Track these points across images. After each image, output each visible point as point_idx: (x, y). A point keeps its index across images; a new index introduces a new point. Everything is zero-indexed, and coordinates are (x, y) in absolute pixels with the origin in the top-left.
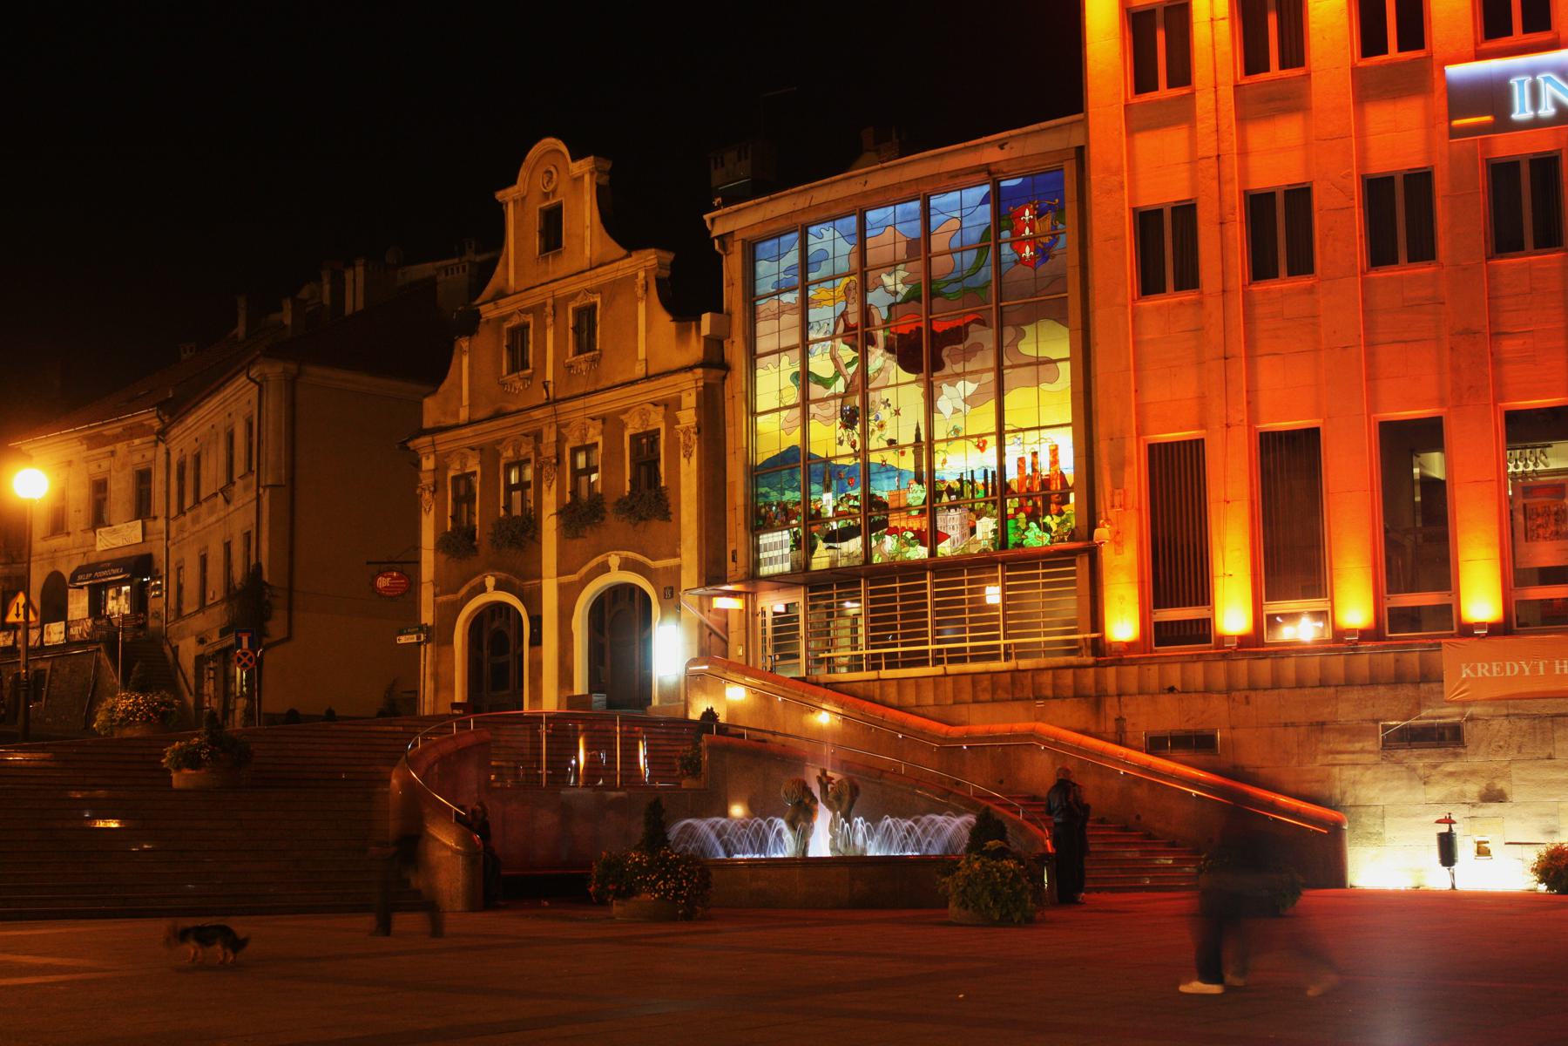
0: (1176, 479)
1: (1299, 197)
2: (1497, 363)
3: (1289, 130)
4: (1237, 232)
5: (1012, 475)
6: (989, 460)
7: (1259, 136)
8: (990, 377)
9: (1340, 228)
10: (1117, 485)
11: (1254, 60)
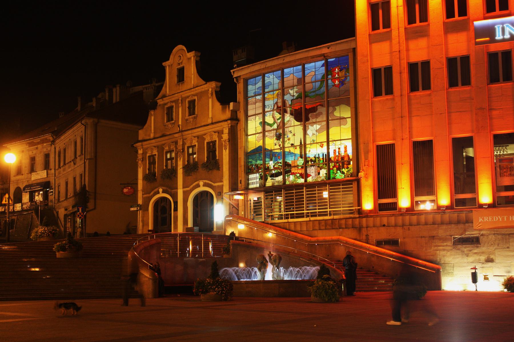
0: (386, 157)
1: (426, 64)
2: (491, 119)
3: (422, 43)
4: (406, 76)
5: (332, 155)
6: (324, 150)
7: (413, 44)
8: (324, 123)
9: (439, 74)
10: (366, 158)
11: (411, 20)
